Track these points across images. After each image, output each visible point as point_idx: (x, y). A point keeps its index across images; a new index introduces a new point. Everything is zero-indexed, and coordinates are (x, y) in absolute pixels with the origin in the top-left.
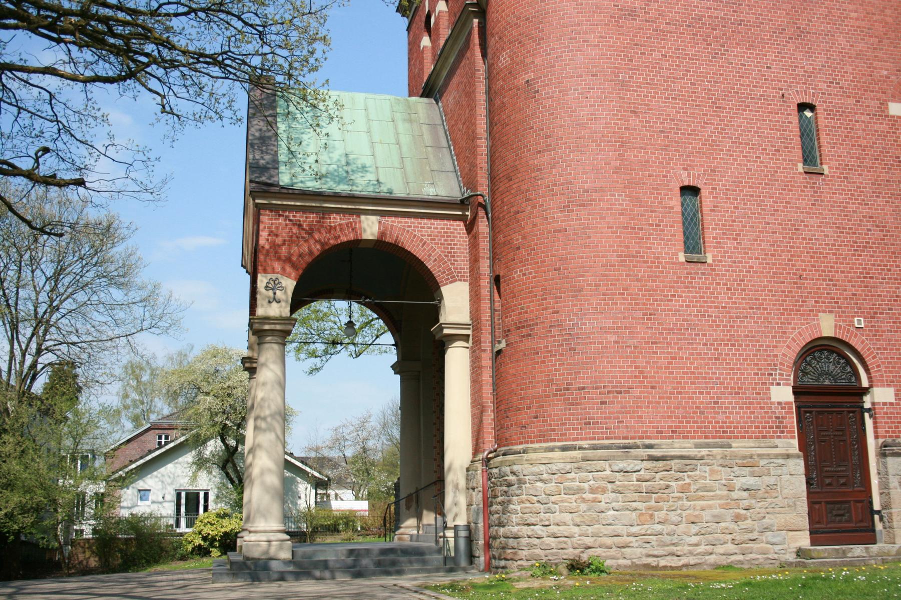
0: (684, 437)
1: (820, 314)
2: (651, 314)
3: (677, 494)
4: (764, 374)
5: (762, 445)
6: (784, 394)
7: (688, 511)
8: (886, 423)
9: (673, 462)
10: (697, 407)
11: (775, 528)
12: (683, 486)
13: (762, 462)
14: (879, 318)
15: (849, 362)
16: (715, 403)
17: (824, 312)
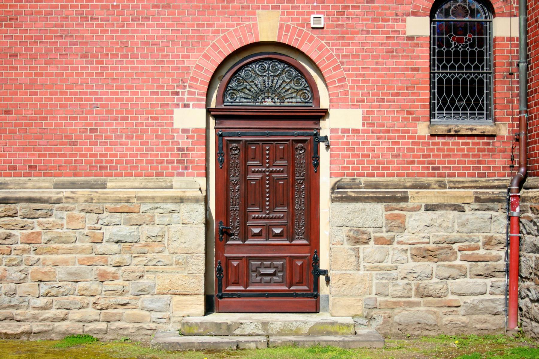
0: (46, 175)
1: (259, 12)
2: (11, 19)
3: (20, 246)
4: (167, 93)
5: (150, 185)
6: (192, 118)
7: (34, 267)
8: (343, 156)
9: (18, 206)
10: (66, 137)
11: (156, 291)
12: (29, 235)
13: (144, 207)
14: (351, 14)
15: (302, 73)
16: (92, 131)
17: (265, 8)
